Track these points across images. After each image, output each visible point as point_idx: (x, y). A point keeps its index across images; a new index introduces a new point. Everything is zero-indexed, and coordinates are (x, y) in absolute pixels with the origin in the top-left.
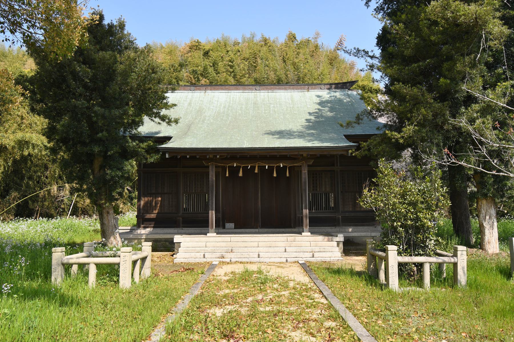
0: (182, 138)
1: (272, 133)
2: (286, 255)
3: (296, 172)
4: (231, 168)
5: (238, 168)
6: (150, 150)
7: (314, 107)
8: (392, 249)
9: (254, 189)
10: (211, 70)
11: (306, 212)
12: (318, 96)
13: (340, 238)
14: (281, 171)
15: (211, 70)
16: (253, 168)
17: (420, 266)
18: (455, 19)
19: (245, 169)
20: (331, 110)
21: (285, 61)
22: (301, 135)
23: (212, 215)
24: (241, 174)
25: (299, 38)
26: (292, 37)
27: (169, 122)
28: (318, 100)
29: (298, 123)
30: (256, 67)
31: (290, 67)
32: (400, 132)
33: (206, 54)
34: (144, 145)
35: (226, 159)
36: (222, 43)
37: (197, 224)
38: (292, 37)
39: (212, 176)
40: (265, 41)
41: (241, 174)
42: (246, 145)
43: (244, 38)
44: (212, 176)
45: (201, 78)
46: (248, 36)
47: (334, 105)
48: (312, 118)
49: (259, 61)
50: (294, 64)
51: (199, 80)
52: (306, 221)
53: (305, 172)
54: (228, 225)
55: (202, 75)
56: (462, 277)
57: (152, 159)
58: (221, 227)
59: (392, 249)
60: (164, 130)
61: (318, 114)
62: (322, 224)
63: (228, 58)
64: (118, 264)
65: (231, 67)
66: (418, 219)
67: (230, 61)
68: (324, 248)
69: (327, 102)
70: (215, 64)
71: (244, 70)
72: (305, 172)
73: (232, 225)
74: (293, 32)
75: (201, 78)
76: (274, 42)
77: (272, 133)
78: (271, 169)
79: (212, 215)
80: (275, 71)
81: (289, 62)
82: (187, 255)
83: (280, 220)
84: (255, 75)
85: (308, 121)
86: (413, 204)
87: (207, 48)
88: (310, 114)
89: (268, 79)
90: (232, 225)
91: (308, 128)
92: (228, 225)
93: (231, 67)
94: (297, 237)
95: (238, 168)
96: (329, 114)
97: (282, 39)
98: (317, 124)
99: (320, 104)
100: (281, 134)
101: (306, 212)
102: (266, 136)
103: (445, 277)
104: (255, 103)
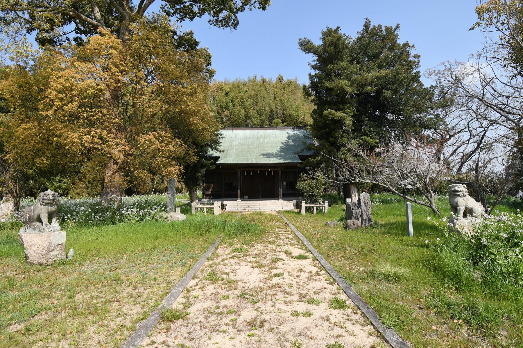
1: (264, 155)
2: (271, 208)
3: (276, 173)
4: (247, 171)
5: (250, 171)
6: (213, 164)
8: (304, 202)
9: (257, 181)
10: (230, 105)
11: (281, 190)
12: (288, 133)
13: (295, 201)
15: (230, 105)
17: (313, 207)
20: (293, 141)
21: (275, 97)
22: (276, 156)
23: (239, 192)
25: (285, 79)
26: (280, 79)
27: (220, 151)
29: (275, 149)
30: (257, 103)
31: (279, 103)
32: (315, 159)
33: (227, 94)
34: (210, 162)
35: (245, 167)
36: (236, 86)
37: (233, 197)
38: (280, 79)
40: (264, 81)
42: (254, 162)
44: (239, 175)
45: (224, 110)
46: (252, 77)
47: (294, 138)
48: (283, 145)
49: (259, 99)
50: (281, 100)
51: (223, 111)
52: (281, 196)
53: (280, 173)
54: (245, 197)
55: (225, 108)
56: (326, 211)
57: (213, 167)
58: (243, 198)
59: (304, 202)
60: (215, 154)
61: (286, 144)
62: (286, 196)
63: (240, 97)
64: (214, 208)
65: (243, 102)
66: (313, 192)
67: (242, 99)
68: (289, 205)
69: (292, 136)
70: (232, 101)
71: (250, 105)
72: (280, 173)
73: (247, 197)
74: (281, 75)
75: (224, 110)
76: (269, 81)
77: (264, 155)
78: (265, 172)
79: (239, 192)
80: (269, 105)
81: (278, 99)
82: (230, 209)
83: (270, 195)
84: (257, 108)
85: (281, 147)
86: (312, 187)
87: (228, 90)
88: (282, 143)
89: (265, 110)
90: (247, 197)
92: (245, 197)
93: (243, 102)
94: (277, 201)
95: (250, 171)
96: (292, 143)
97: (274, 80)
98: (285, 150)
99: (288, 138)
100: (268, 155)
101: (281, 190)
103: (320, 211)
104: (258, 138)
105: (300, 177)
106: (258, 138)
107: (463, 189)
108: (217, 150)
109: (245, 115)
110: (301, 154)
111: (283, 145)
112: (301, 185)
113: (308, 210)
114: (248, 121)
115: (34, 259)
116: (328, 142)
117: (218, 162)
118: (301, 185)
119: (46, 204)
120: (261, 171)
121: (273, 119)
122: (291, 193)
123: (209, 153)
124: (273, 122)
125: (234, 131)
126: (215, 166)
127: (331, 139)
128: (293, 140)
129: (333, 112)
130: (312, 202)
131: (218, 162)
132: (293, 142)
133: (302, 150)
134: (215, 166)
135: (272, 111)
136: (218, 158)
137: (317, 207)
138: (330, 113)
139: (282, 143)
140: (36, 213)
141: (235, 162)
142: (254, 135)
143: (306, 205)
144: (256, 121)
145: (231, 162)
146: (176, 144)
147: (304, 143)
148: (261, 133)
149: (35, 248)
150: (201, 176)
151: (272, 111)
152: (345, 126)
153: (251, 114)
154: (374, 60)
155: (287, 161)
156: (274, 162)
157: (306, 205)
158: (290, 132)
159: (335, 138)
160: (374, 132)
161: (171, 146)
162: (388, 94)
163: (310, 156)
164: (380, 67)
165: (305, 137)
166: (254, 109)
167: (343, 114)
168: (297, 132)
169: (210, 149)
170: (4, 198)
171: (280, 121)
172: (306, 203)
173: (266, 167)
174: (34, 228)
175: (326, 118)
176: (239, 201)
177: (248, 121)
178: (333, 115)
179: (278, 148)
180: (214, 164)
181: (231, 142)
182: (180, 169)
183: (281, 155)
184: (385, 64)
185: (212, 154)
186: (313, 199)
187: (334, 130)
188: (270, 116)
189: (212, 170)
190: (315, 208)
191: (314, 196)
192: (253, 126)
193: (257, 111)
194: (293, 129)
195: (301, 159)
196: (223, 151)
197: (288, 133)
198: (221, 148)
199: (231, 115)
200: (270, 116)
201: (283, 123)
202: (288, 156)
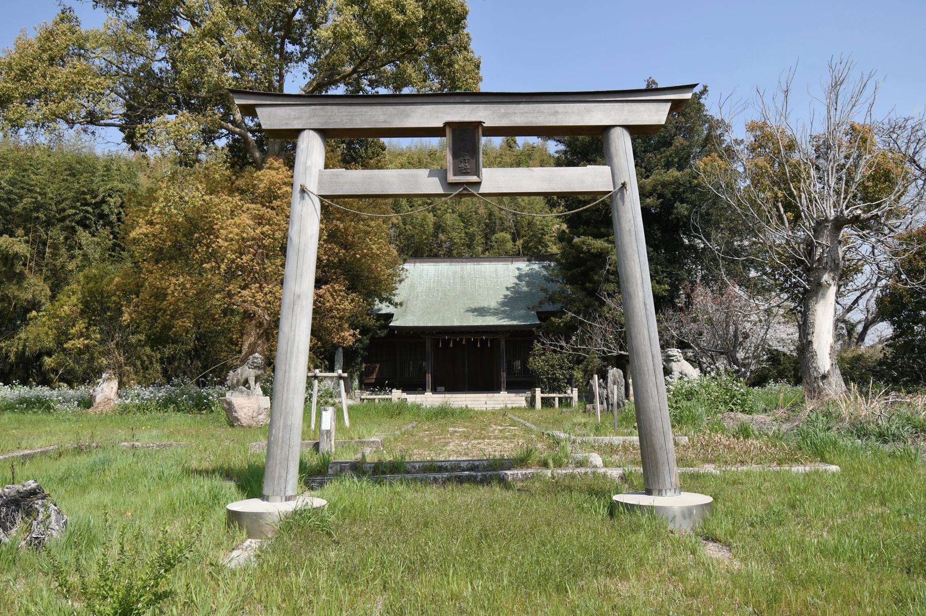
0: (407, 317)
4: (444, 341)
5: (449, 340)
7: (512, 281)
11: (504, 375)
12: (518, 269)
14: (483, 343)
16: (461, 340)
18: (589, 251)
19: (455, 341)
22: (495, 313)
23: (429, 378)
24: (451, 345)
27: (396, 305)
28: (517, 273)
29: (493, 300)
35: (440, 333)
36: (416, 160)
39: (428, 347)
41: (451, 345)
42: (456, 323)
43: (763, 139)
44: (428, 347)
48: (508, 293)
52: (504, 385)
53: (503, 343)
57: (383, 333)
58: (434, 391)
60: (385, 308)
61: (515, 289)
62: (514, 387)
66: (554, 374)
68: (518, 400)
69: (526, 275)
72: (503, 343)
73: (443, 388)
78: (476, 340)
79: (429, 378)
83: (486, 383)
85: (506, 296)
88: (507, 289)
89: (476, 213)
90: (443, 388)
91: (503, 304)
92: (439, 388)
95: (449, 340)
96: (525, 289)
98: (513, 301)
99: (519, 278)
100: (481, 311)
102: (468, 314)
103: (566, 402)
104: (462, 278)
105: (532, 349)
106: (462, 278)
107: (677, 354)
108: (390, 302)
109: (435, 224)
110: (540, 310)
111: (508, 293)
112: (537, 363)
113: (547, 402)
114: (442, 237)
115: (245, 422)
116: (585, 289)
117: (391, 324)
118: (537, 363)
119: (255, 367)
120: (468, 340)
121: (494, 232)
122: (521, 382)
123: (376, 307)
124: (493, 238)
125: (418, 265)
126: (386, 331)
127: (587, 285)
128: (527, 282)
129: (590, 240)
130: (552, 390)
131: (391, 324)
132: (528, 286)
133: (541, 303)
134: (386, 331)
135: (491, 214)
136: (390, 316)
137: (560, 399)
138: (583, 243)
139: (507, 289)
140: (244, 377)
141: (421, 324)
142: (455, 273)
143: (543, 395)
144: (458, 236)
145: (416, 325)
146: (353, 300)
147: (544, 290)
148: (469, 268)
149: (245, 410)
150: (362, 348)
151: (491, 214)
152: (610, 265)
153: (448, 222)
154: (662, 149)
155: (515, 323)
156: (491, 324)
157: (543, 395)
158: (523, 266)
159: (594, 282)
160: (663, 272)
161: (346, 303)
162: (682, 209)
163: (554, 314)
164: (668, 166)
165: (547, 279)
166: (453, 212)
167: (606, 245)
168: (536, 266)
169: (377, 302)
170: (104, 375)
171: (508, 236)
172: (542, 392)
173: (478, 332)
174: (242, 392)
175: (578, 249)
176: (429, 394)
177: (442, 237)
178: (589, 245)
179: (500, 298)
180: (386, 326)
181: (412, 286)
182: (354, 334)
183: (504, 312)
184: (676, 160)
185: (380, 310)
186: (554, 385)
187: (593, 269)
188: (487, 225)
189: (381, 337)
190: (557, 399)
191: (556, 379)
192: (451, 255)
193: (460, 216)
194: (529, 260)
195: (540, 319)
196: (401, 304)
197: (518, 269)
198: (397, 299)
199: (405, 224)
200: (487, 225)
201: (514, 240)
202: (516, 313)
